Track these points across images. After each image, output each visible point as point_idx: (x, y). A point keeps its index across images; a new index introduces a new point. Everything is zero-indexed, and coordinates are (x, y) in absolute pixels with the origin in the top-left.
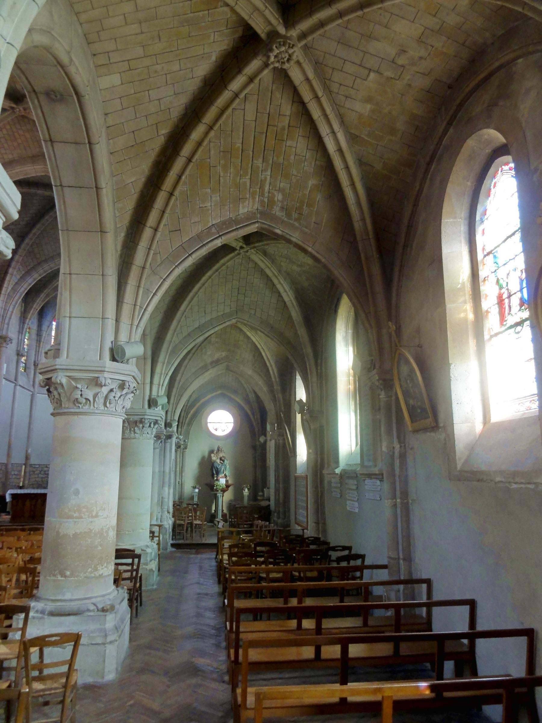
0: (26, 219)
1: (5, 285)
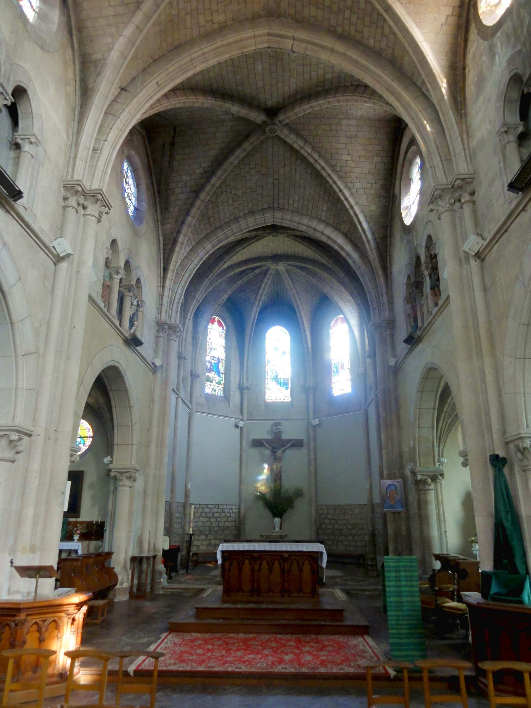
1: (174, 258)
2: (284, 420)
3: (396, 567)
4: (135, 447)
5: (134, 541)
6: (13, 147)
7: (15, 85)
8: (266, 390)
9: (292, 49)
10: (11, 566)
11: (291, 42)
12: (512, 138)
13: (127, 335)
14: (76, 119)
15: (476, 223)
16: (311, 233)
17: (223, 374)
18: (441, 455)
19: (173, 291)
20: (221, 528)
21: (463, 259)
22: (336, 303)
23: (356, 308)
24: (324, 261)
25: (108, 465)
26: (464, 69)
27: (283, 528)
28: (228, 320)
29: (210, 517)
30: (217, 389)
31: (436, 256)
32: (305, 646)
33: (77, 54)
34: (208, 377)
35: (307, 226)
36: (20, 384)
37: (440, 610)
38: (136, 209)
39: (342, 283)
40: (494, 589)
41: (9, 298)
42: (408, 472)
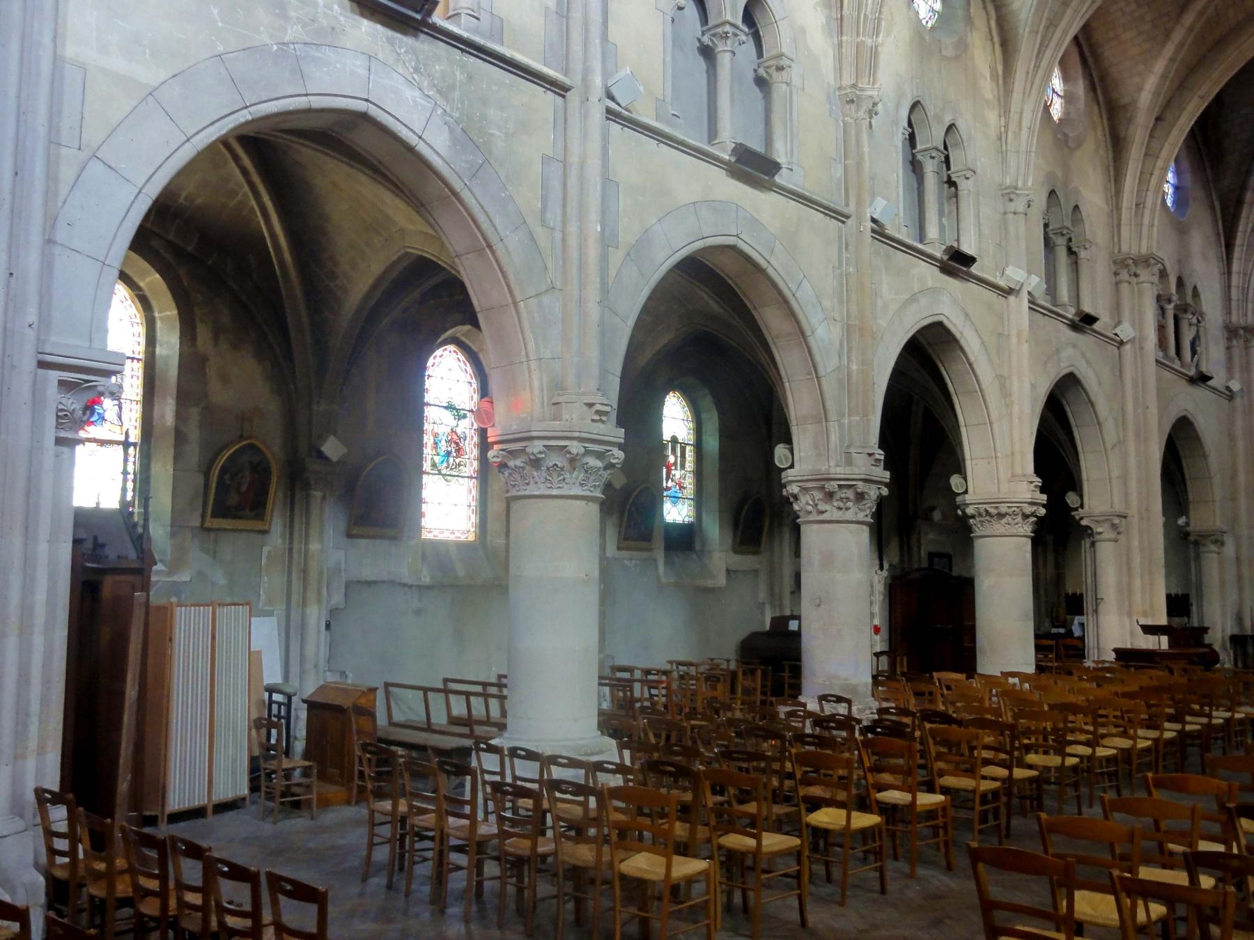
1: (1241, 228)
4: (1218, 504)
14: (1112, 179)
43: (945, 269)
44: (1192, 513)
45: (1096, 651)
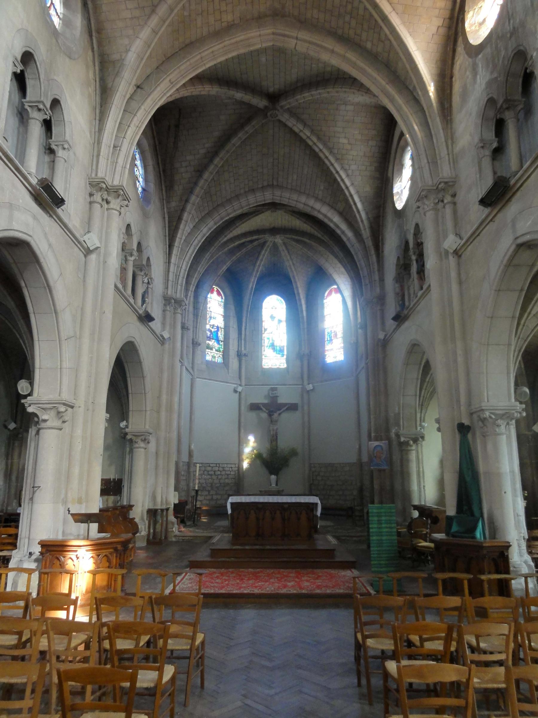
0: (207, 145)
1: (179, 235)
2: (281, 385)
3: (378, 513)
4: (148, 413)
5: (149, 496)
6: (47, 152)
7: (52, 99)
8: (263, 357)
9: (295, 48)
10: (69, 513)
11: (294, 41)
12: (488, 152)
13: (141, 312)
14: (97, 118)
15: (456, 225)
16: (308, 210)
17: (222, 341)
18: (422, 420)
19: (179, 267)
20: (222, 485)
21: (443, 254)
22: (331, 275)
23: (349, 280)
24: (319, 236)
25: (124, 429)
26: (451, 77)
27: (278, 484)
28: (228, 290)
29: (211, 475)
30: (217, 356)
31: (422, 243)
32: (304, 576)
33: (96, 56)
34: (208, 344)
35: (305, 204)
36: (64, 366)
37: (416, 549)
38: (144, 190)
39: (336, 257)
40: (455, 528)
41: (54, 292)
42: (393, 435)
43: (37, 198)
44: (130, 420)
45: (27, 540)
